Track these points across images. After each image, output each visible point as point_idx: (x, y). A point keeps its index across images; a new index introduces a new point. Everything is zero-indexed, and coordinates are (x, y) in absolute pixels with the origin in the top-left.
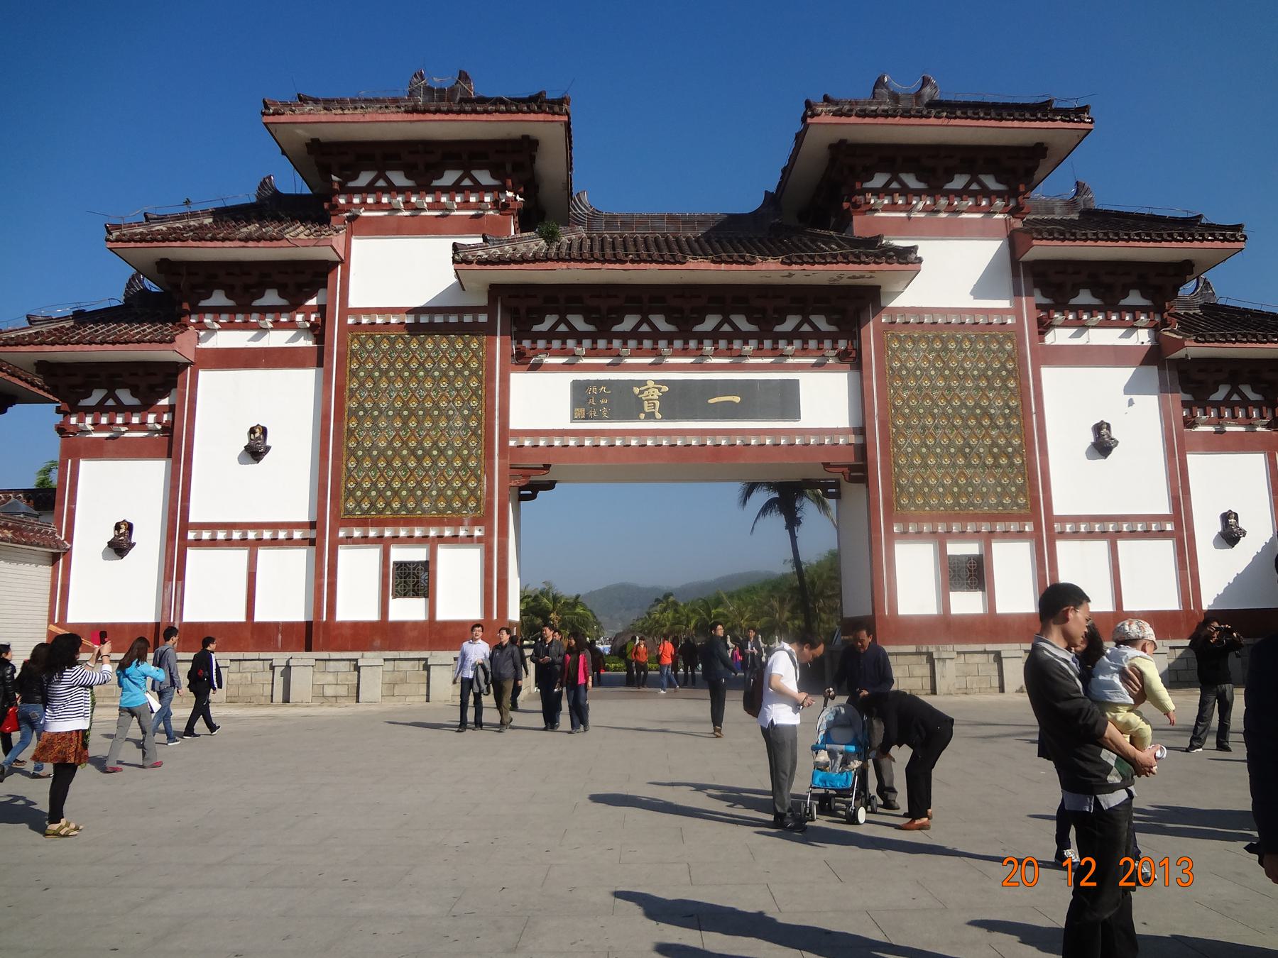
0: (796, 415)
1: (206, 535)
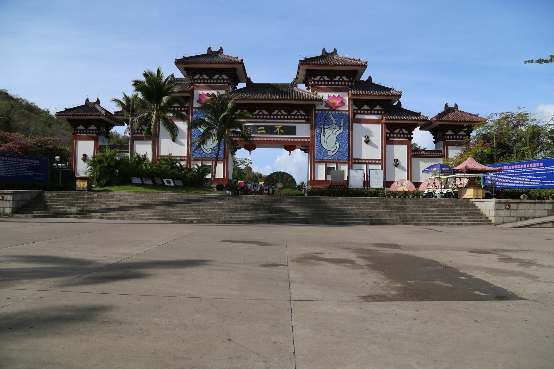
0: (295, 134)
1: (377, 162)
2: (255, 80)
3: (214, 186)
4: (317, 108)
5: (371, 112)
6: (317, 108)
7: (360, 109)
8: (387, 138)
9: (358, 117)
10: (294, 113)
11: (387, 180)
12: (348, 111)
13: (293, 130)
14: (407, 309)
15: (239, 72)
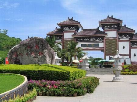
0: (82, 44)
2: (84, 28)
3: (35, 48)
4: (106, 37)
5: (125, 37)
6: (106, 37)
7: (121, 37)
8: (131, 46)
9: (120, 39)
10: (91, 39)
11: (132, 61)
12: (117, 37)
13: (98, 45)
14: (63, 66)
15: (79, 25)
